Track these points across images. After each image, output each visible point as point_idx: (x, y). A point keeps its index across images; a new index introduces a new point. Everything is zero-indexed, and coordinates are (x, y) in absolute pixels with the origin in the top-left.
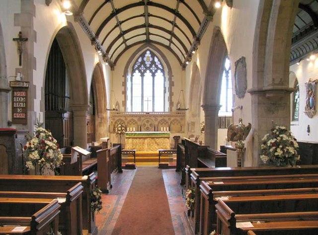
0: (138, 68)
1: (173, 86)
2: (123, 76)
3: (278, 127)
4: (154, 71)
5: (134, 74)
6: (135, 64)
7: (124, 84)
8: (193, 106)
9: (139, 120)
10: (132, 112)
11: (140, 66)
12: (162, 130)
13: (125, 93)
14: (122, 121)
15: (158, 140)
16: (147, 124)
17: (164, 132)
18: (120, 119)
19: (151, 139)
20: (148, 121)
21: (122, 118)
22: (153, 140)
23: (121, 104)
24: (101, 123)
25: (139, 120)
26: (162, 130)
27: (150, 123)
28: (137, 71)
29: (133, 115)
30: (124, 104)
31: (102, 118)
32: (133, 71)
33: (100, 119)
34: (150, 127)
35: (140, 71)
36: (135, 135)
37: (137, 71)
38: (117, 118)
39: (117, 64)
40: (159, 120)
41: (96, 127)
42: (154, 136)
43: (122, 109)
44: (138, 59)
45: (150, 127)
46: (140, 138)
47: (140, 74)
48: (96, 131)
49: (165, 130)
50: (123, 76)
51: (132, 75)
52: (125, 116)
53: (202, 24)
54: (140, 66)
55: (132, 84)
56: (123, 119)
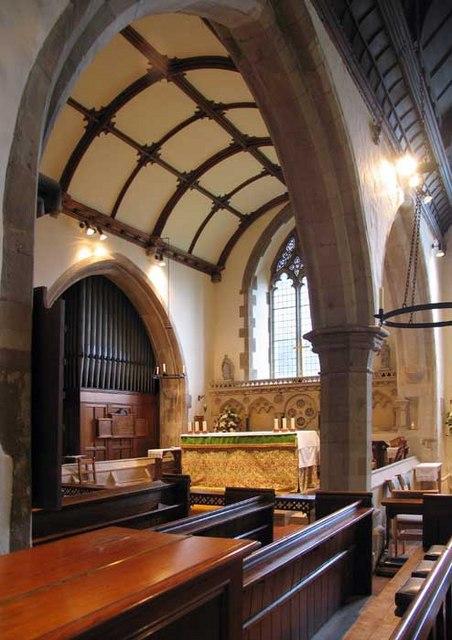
0: (286, 269)
1: (241, 307)
2: (241, 293)
3: (123, 446)
4: (297, 272)
5: (278, 284)
6: (278, 258)
7: (245, 311)
8: (406, 352)
9: (279, 400)
10: (274, 381)
11: (290, 262)
12: (276, 426)
13: (245, 333)
14: (238, 404)
15: (264, 457)
16: (303, 410)
17: (280, 433)
18: (232, 400)
19: (243, 453)
20: (301, 403)
21: (236, 397)
22: (249, 456)
23: (236, 361)
24: (170, 411)
25: (279, 400)
26: (276, 426)
27: (306, 407)
28: (284, 276)
29: (261, 389)
30: (245, 360)
31: (173, 400)
32: (274, 277)
33: (167, 402)
34: (307, 418)
35: (291, 275)
36: (224, 442)
37: (284, 276)
38: (227, 398)
39: (228, 264)
40: (223, 402)
41: (162, 423)
42: (251, 445)
43: (239, 374)
44: (286, 243)
45: (307, 418)
46: (217, 450)
47: (291, 282)
48: (161, 430)
49: (197, 429)
50: (241, 293)
51: (272, 289)
52: (243, 392)
53: (63, 100)
54: (290, 262)
55: (272, 311)
56: (239, 398)
